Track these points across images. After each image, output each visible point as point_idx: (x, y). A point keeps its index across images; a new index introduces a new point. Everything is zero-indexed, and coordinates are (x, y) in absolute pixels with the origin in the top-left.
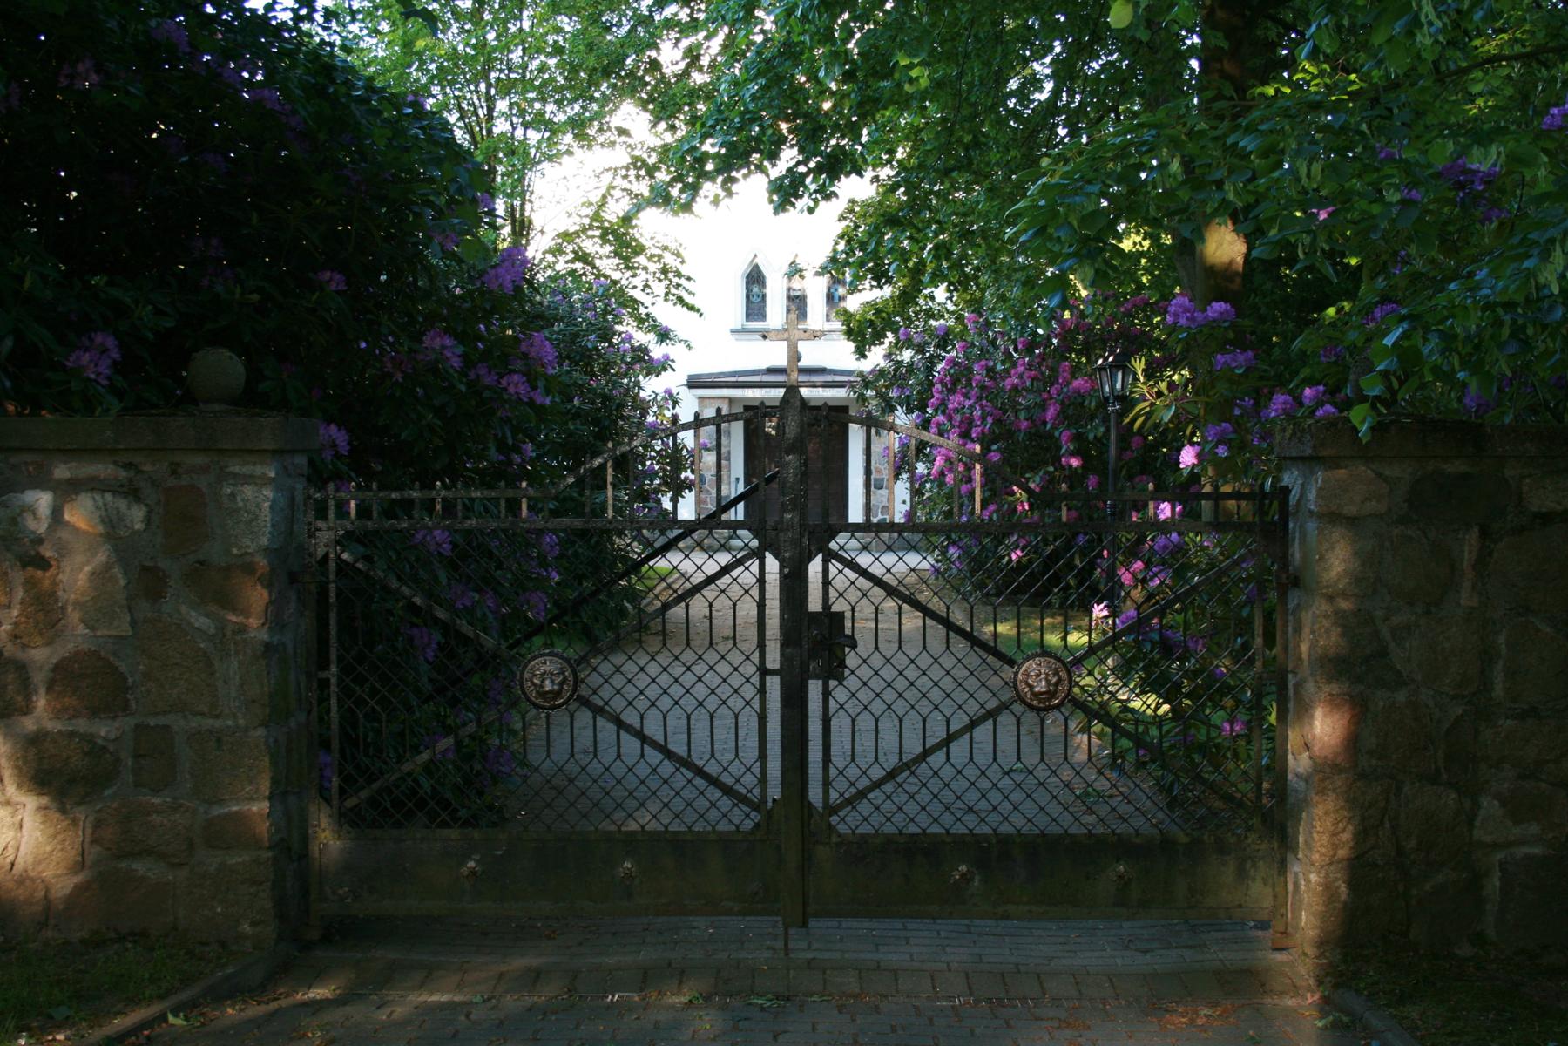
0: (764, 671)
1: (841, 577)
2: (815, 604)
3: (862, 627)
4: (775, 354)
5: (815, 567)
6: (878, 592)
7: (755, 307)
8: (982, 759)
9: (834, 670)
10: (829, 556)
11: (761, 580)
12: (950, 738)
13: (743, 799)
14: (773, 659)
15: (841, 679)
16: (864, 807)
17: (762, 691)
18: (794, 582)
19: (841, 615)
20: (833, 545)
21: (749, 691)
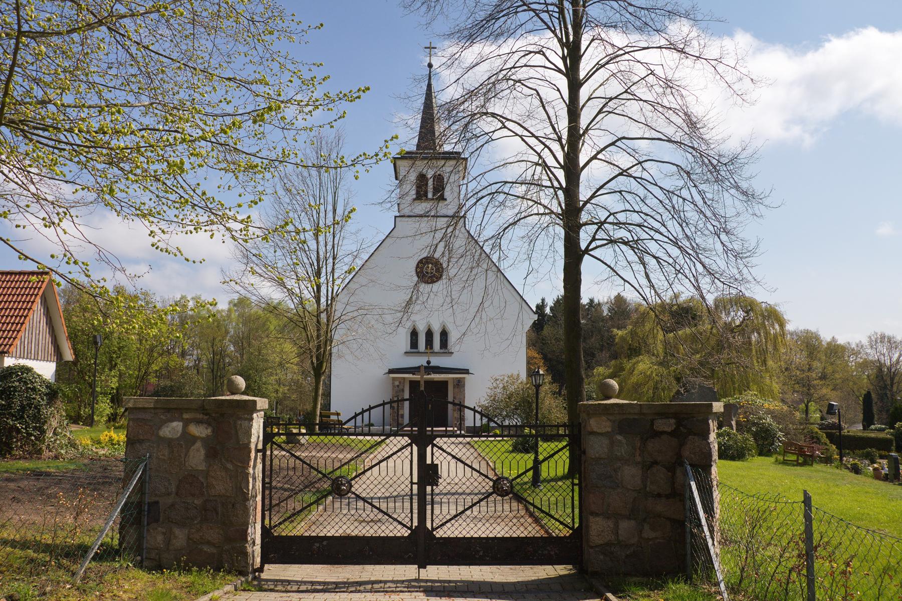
0: (412, 483)
1: (437, 452)
2: (429, 461)
3: (443, 471)
4: (420, 361)
5: (415, 523)
6: (450, 457)
7: (414, 344)
8: (383, 474)
9: (434, 482)
10: (434, 445)
11: (411, 453)
12: (471, 507)
13: (404, 526)
14: (415, 480)
15: (437, 485)
16: (399, 446)
17: (573, 491)
18: (422, 456)
19: (437, 465)
20: (409, 532)
21: (569, 490)
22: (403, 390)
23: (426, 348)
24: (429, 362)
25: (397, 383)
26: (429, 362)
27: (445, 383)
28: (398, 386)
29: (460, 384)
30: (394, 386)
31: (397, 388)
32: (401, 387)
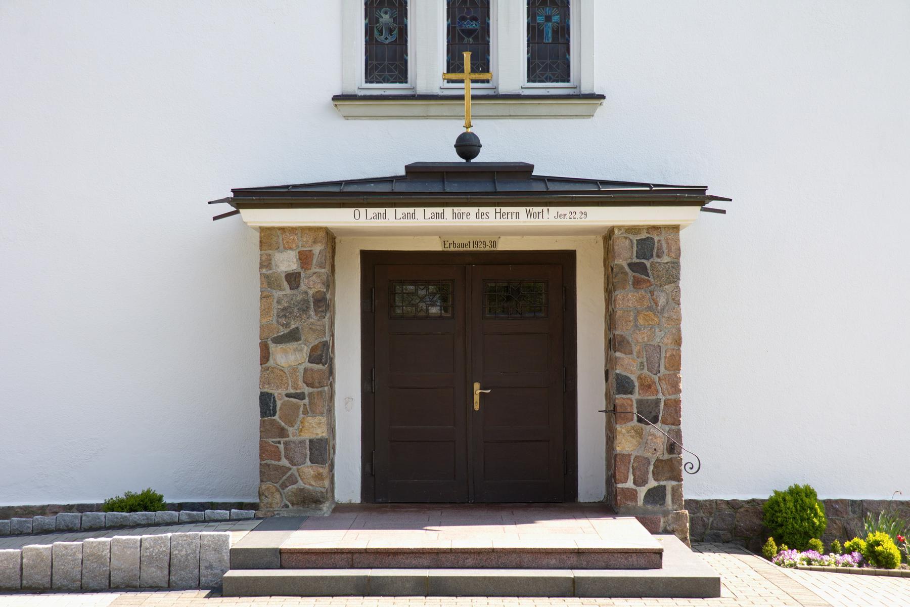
22: (323, 304)
23: (454, 65)
24: (467, 146)
25: (287, 262)
26: (467, 146)
27: (560, 265)
28: (293, 279)
29: (647, 265)
30: (269, 281)
31: (290, 310)
32: (311, 285)
